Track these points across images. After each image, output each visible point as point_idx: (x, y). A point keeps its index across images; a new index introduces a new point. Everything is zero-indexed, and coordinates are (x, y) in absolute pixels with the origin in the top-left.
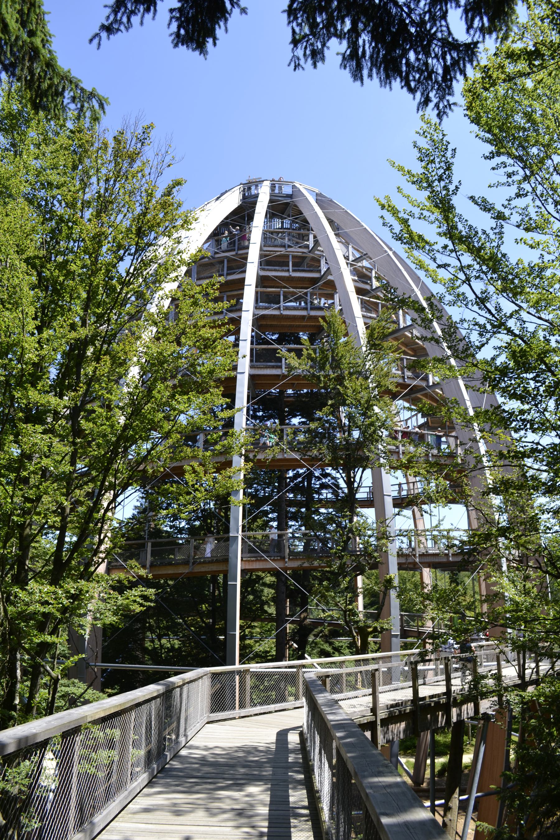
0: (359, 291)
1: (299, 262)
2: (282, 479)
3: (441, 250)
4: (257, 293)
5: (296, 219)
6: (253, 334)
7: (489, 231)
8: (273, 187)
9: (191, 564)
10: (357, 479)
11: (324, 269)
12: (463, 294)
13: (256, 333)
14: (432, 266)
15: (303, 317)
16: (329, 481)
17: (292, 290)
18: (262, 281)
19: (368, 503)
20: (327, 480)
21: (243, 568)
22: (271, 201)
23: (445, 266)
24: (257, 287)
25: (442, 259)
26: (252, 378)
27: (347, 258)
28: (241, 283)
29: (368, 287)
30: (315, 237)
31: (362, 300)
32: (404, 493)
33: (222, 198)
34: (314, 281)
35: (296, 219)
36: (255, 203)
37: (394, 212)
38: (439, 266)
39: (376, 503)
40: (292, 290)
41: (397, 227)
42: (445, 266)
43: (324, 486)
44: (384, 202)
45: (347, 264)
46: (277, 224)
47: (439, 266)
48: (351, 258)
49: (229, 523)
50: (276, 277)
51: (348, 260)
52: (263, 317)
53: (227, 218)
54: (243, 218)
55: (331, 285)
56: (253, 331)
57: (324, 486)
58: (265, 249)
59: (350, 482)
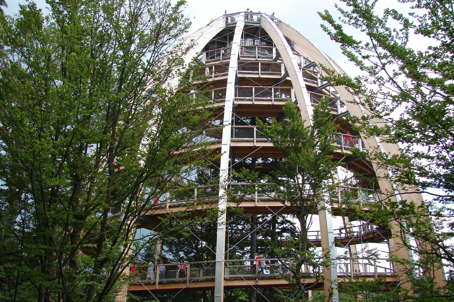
0: (309, 88)
1: (266, 67)
2: (254, 222)
3: (364, 47)
4: (236, 89)
5: (264, 38)
6: (234, 118)
7: (398, 30)
8: (246, 17)
9: (188, 282)
10: (308, 221)
11: (283, 73)
12: (381, 77)
13: (236, 117)
14: (360, 59)
15: (269, 106)
16: (289, 226)
17: (262, 87)
18: (239, 81)
19: (318, 243)
20: (287, 225)
21: (225, 285)
22: (245, 26)
23: (367, 57)
24: (235, 85)
25: (365, 52)
26: (232, 149)
27: (300, 65)
28: (225, 82)
29: (315, 85)
30: (277, 50)
31: (311, 94)
32: (343, 235)
33: (211, 24)
34: (276, 81)
35: (264, 38)
36: (235, 27)
37: (331, 21)
38: (364, 57)
39: (322, 243)
40: (262, 87)
41: (334, 31)
42: (367, 57)
43: (284, 230)
44: (324, 13)
45: (300, 69)
46: (249, 42)
47: (364, 57)
48: (303, 66)
49: (215, 251)
50: (250, 78)
51: (301, 66)
52: (240, 105)
53: (214, 38)
54: (225, 38)
55: (289, 83)
56: (233, 116)
57: (284, 230)
58: (241, 59)
59: (303, 223)
